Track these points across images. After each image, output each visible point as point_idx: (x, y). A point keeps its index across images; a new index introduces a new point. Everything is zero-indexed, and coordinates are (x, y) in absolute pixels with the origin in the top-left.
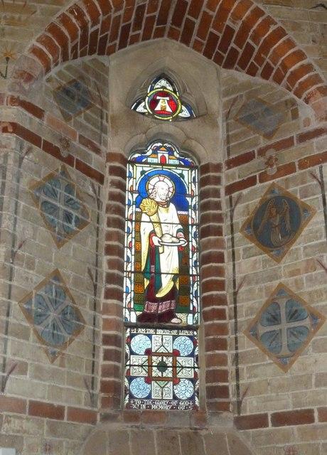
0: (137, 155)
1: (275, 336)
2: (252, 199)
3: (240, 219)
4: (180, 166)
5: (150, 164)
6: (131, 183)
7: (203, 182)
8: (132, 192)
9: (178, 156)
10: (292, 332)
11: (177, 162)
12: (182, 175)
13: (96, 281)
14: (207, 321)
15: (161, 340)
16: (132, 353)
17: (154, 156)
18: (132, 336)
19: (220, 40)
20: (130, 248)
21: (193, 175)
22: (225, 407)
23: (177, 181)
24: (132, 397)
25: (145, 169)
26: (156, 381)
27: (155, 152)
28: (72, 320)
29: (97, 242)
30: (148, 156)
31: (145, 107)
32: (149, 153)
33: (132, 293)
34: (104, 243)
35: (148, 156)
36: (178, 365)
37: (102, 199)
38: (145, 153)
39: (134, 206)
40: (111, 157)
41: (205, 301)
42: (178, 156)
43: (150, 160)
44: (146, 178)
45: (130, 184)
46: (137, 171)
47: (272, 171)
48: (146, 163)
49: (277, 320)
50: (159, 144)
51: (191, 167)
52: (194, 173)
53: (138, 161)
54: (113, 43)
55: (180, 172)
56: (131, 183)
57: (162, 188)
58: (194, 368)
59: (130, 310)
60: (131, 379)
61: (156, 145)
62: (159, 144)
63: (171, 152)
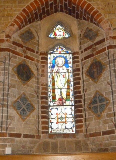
0: (51, 51)
1: (96, 107)
2: (89, 62)
3: (85, 70)
4: (65, 53)
5: (55, 54)
6: (50, 61)
7: (73, 58)
8: (50, 63)
9: (65, 50)
10: (101, 106)
11: (64, 52)
12: (66, 57)
13: (38, 94)
14: (82, 121)
15: (61, 110)
16: (52, 115)
17: (57, 51)
18: (51, 109)
19: (64, 7)
20: (50, 82)
21: (70, 56)
22: (82, 131)
23: (65, 58)
24: (52, 128)
25: (54, 56)
26: (60, 123)
27: (57, 49)
28: (31, 108)
29: (38, 73)
30: (55, 51)
31: (53, 36)
32: (55, 50)
33: (51, 96)
34: (40, 95)
35: (55, 51)
36: (66, 117)
37: (39, 95)
38: (54, 50)
39: (51, 68)
40: (41, 54)
41: (75, 98)
42: (65, 50)
43: (55, 53)
44: (55, 59)
45: (49, 61)
46: (51, 57)
47: (94, 53)
48: (54, 54)
49: (96, 102)
50: (58, 47)
51: (69, 53)
52: (71, 55)
53: (52, 53)
54: (87, 16)
55: (66, 55)
56: (50, 61)
57: (60, 61)
58: (72, 118)
59: (51, 102)
60: (52, 123)
61: (57, 47)
62: (58, 47)
63: (62, 49)
